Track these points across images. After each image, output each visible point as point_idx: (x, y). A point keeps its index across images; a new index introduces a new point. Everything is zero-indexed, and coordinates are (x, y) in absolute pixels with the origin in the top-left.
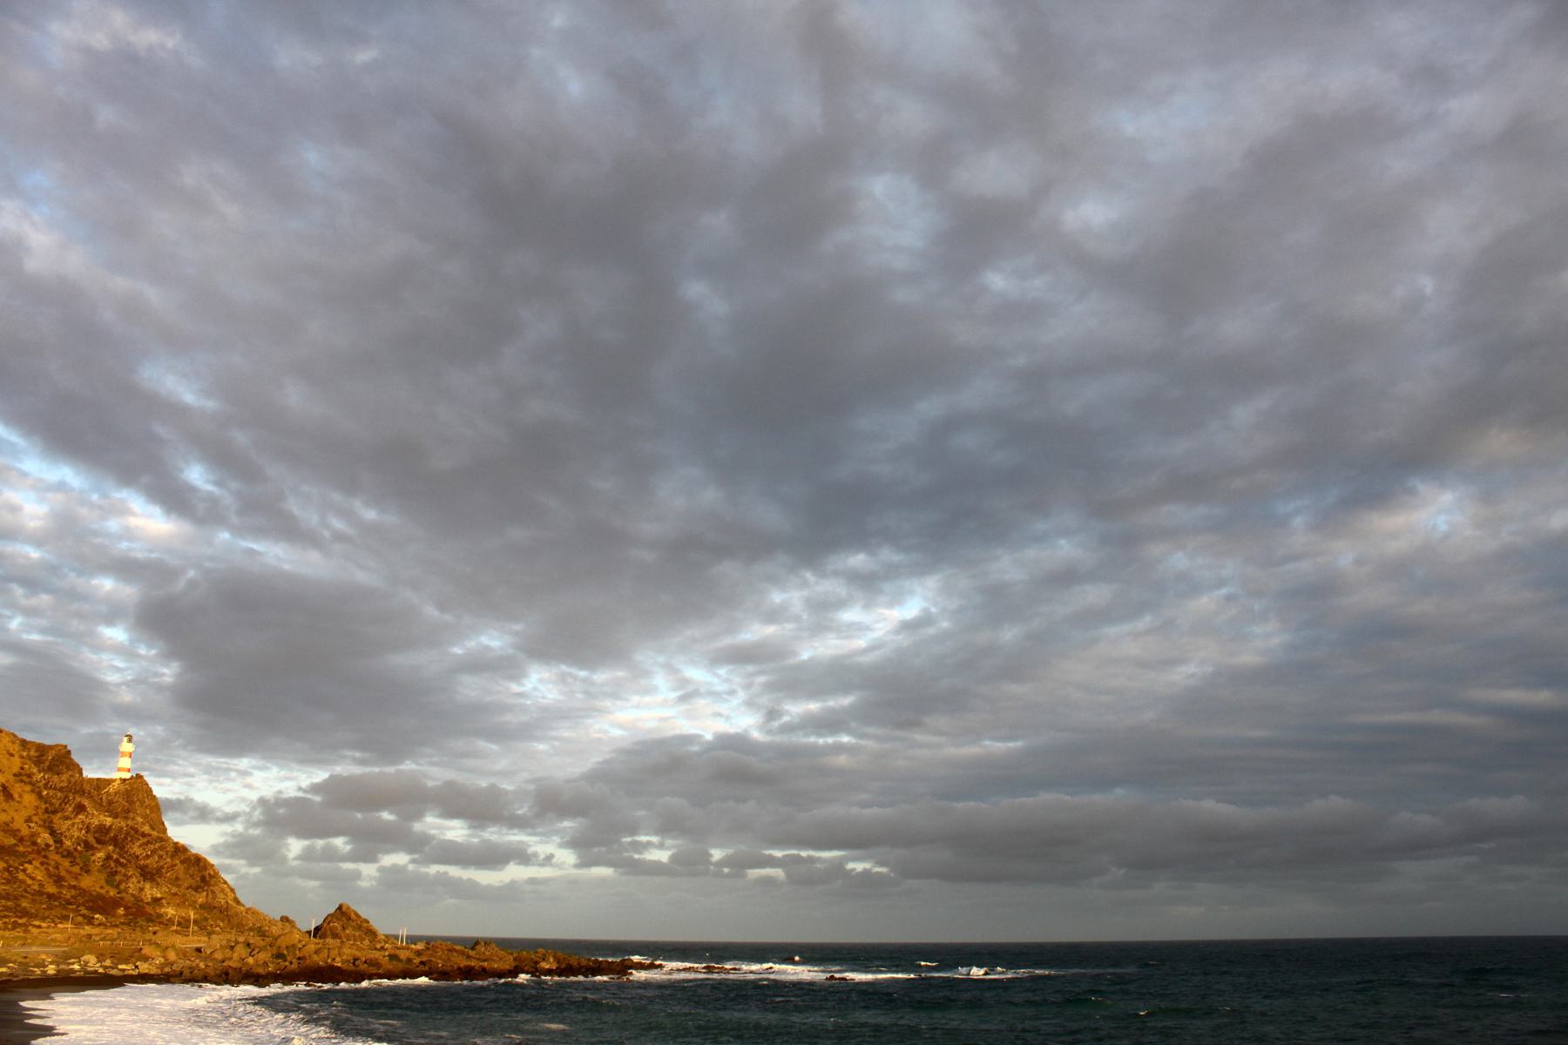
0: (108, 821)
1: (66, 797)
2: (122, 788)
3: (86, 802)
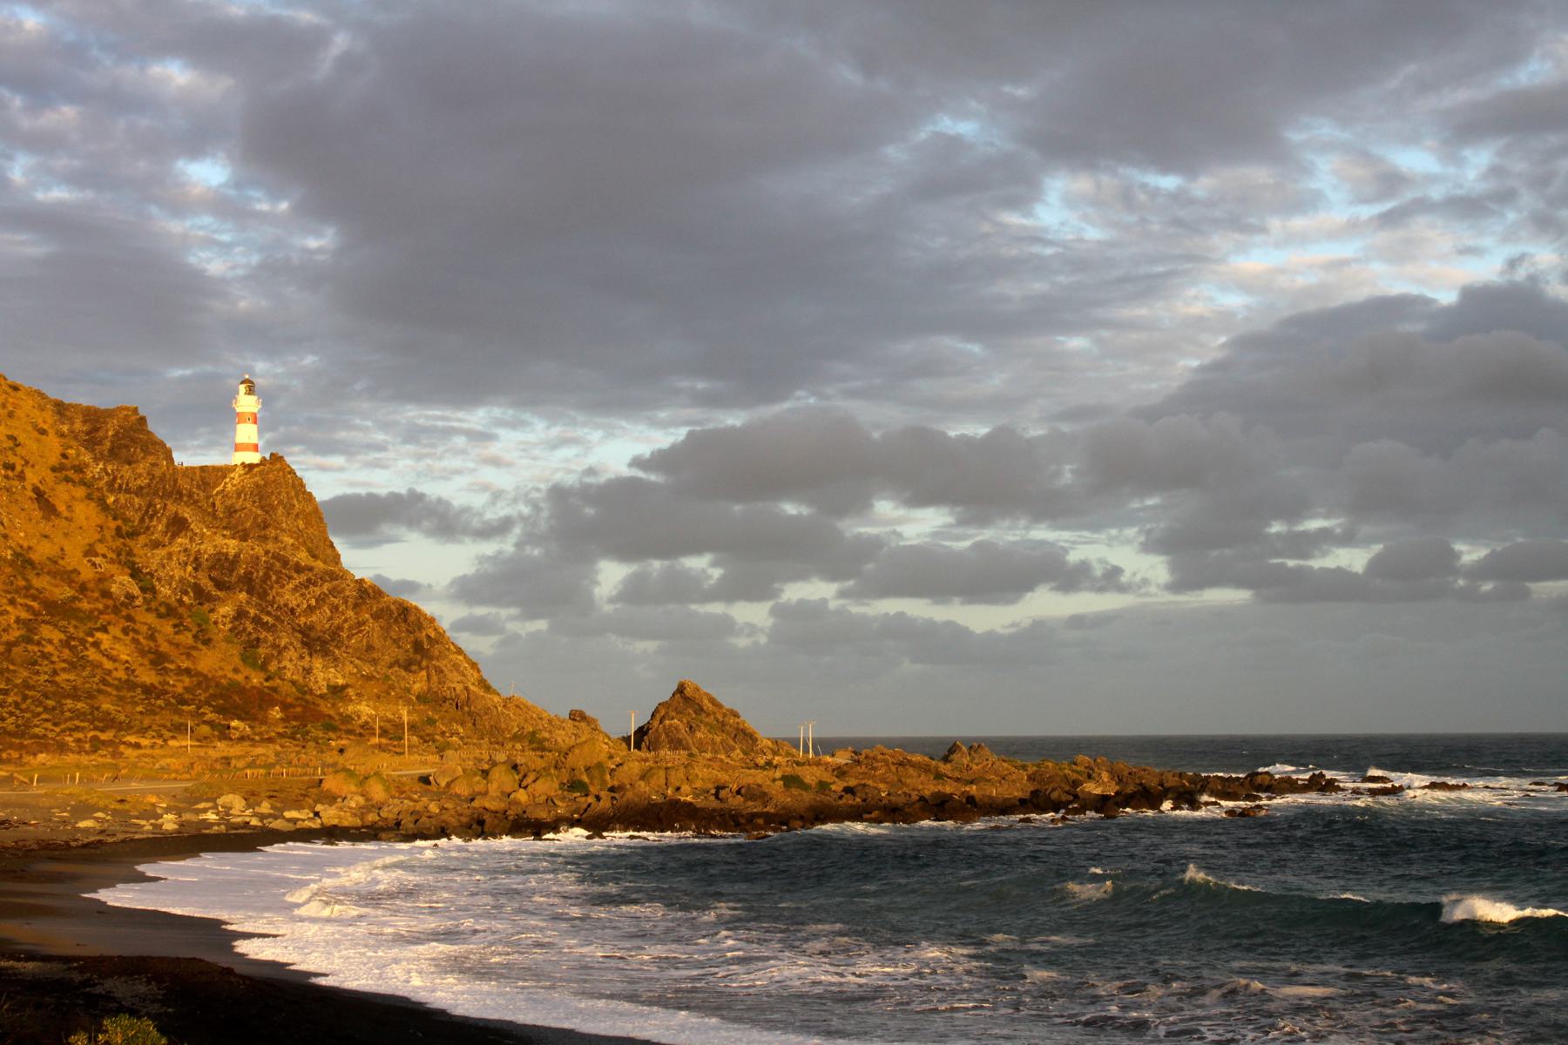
0: (232, 546)
1: (150, 505)
2: (249, 482)
3: (187, 513)
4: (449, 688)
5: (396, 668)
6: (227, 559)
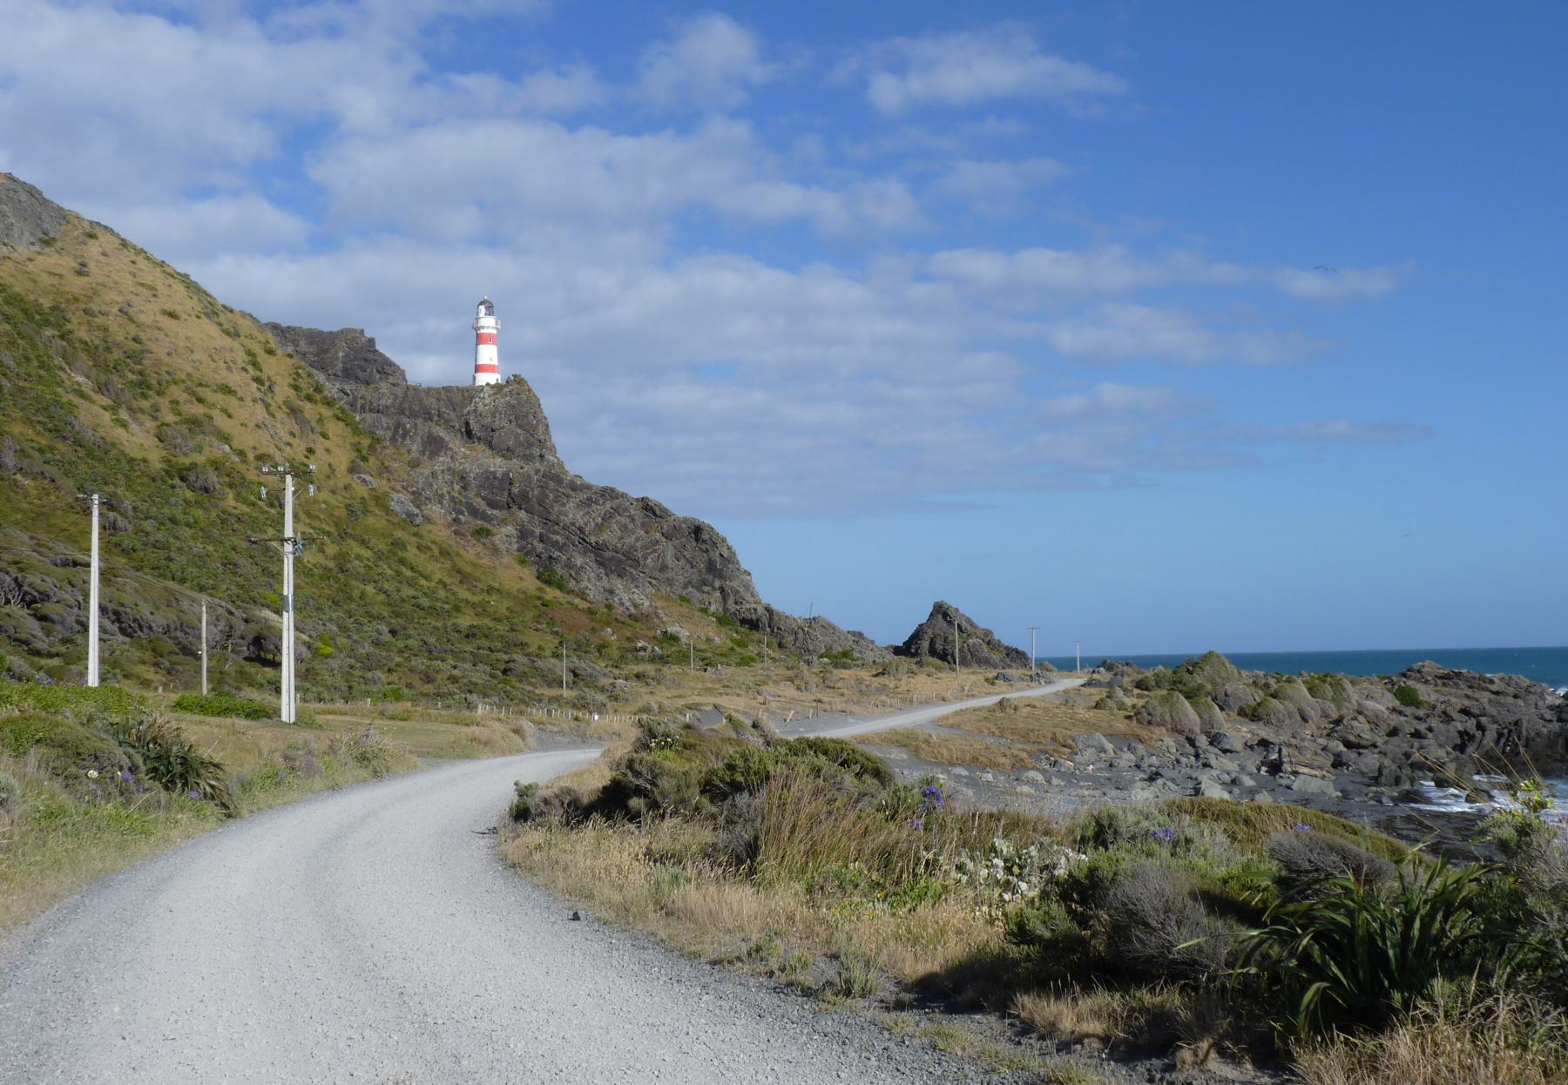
0: (497, 464)
1: (398, 426)
2: (502, 401)
3: (441, 432)
4: (749, 610)
5: (690, 589)
6: (495, 478)
